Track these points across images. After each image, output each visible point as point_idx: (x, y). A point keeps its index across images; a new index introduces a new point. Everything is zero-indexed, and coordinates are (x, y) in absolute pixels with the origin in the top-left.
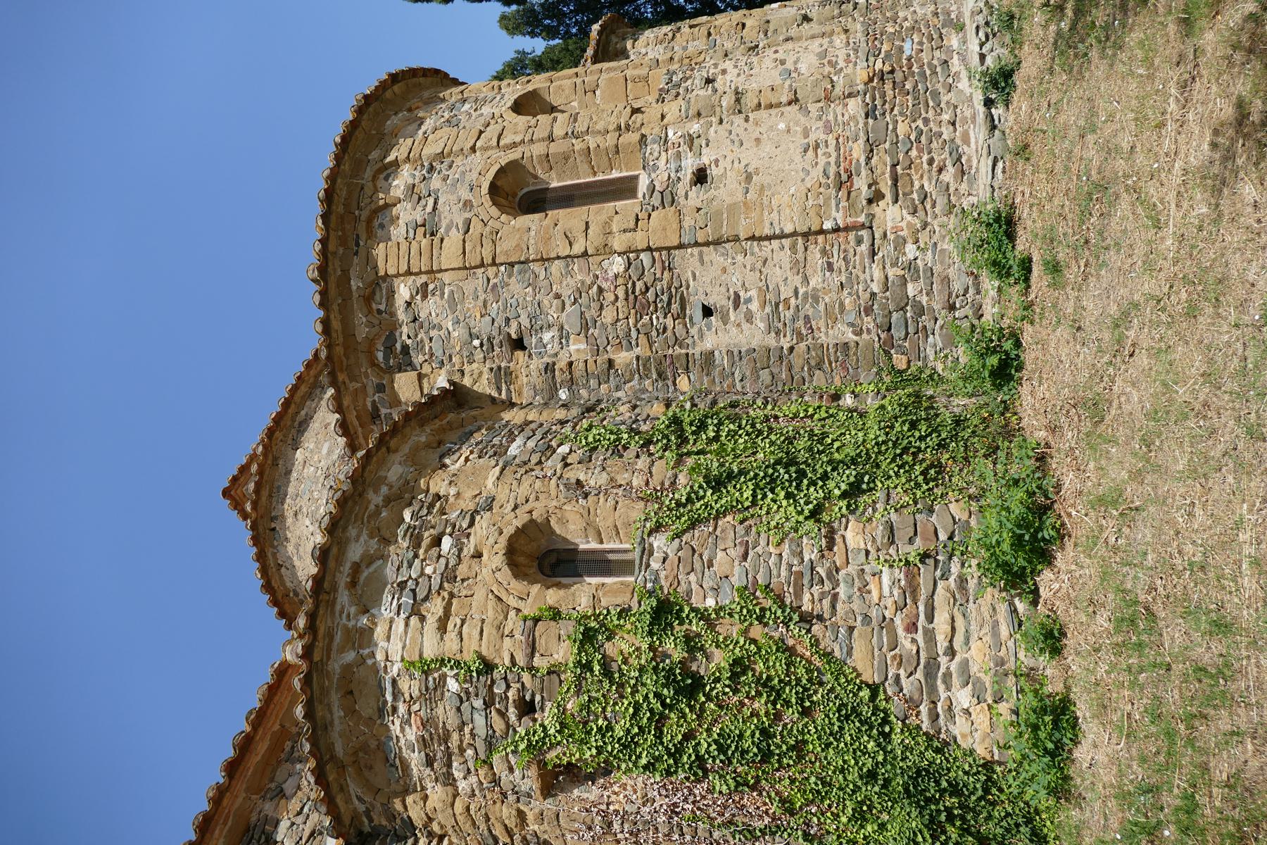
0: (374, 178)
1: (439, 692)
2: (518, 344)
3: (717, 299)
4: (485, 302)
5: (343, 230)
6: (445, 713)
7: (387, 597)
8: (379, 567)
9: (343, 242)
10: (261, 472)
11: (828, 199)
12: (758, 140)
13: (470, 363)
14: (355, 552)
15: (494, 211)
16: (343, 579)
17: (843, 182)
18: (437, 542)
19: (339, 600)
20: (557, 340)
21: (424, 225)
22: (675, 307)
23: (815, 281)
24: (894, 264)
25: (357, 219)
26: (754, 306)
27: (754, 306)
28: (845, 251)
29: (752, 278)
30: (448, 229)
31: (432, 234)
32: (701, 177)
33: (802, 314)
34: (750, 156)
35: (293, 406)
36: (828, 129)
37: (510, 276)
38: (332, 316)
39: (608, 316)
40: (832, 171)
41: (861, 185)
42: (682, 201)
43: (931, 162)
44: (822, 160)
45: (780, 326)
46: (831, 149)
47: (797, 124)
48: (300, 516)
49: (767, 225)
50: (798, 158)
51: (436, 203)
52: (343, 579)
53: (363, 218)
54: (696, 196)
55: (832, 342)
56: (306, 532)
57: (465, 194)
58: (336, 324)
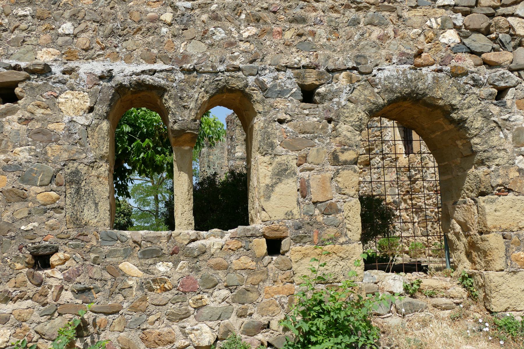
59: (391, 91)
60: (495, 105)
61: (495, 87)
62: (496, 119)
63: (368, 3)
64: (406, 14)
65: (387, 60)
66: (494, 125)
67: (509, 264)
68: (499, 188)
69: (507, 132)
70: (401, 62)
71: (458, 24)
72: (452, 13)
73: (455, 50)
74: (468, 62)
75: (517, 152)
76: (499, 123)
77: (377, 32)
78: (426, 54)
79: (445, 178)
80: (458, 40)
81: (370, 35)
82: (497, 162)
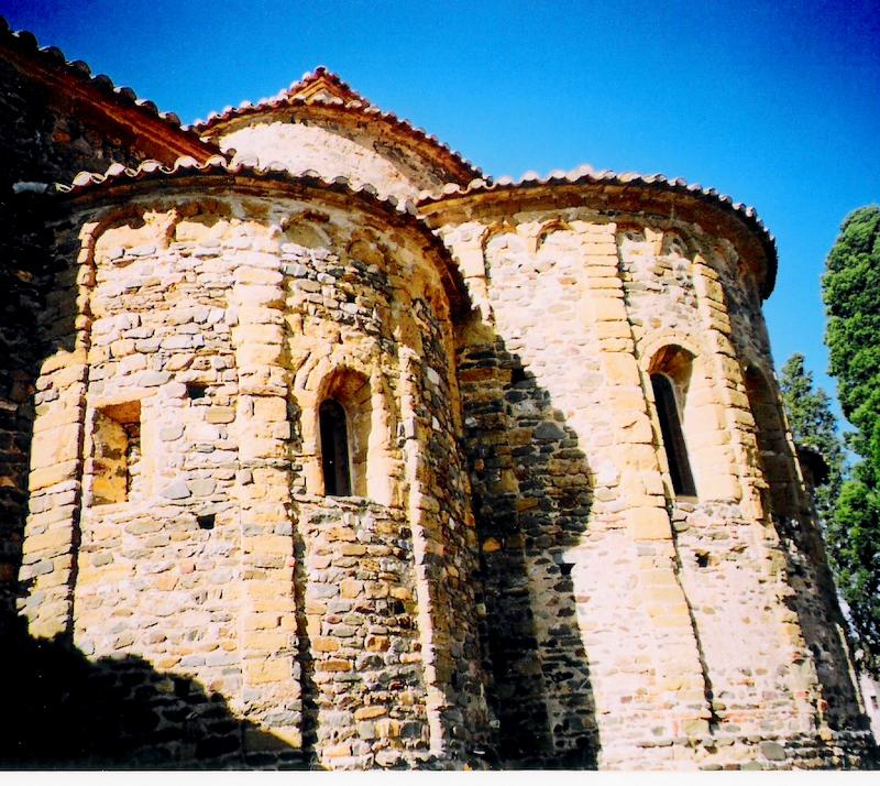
0: (676, 230)
1: (207, 300)
5: (624, 200)
6: (184, 306)
7: (298, 249)
8: (323, 242)
9: (613, 199)
10: (352, 110)
14: (338, 217)
16: (314, 206)
19: (292, 202)
25: (635, 211)
28: (644, 716)
35: (416, 142)
38: (540, 189)
45: (559, 646)
52: (314, 206)
53: (637, 219)
55: (546, 701)
58: (531, 192)
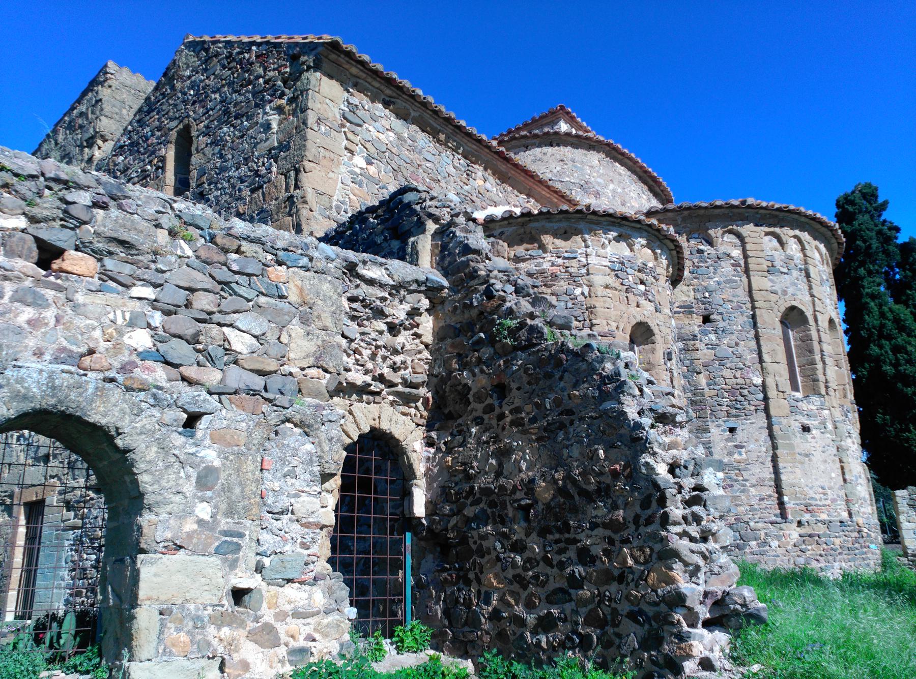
2: (706, 319)
3: (740, 435)
4: (731, 301)
11: (799, 499)
12: (826, 461)
13: (694, 290)
15: (783, 309)
17: (808, 509)
18: (642, 282)
20: (710, 342)
21: (773, 266)
22: (734, 411)
23: (753, 491)
24: (766, 534)
26: (736, 457)
27: (736, 457)
29: (753, 456)
30: (772, 281)
31: (768, 271)
32: (806, 429)
33: (733, 483)
34: (817, 457)
36: (833, 501)
37: (747, 317)
39: (727, 373)
40: (813, 502)
41: (806, 517)
42: (793, 418)
43: (821, 555)
44: (818, 496)
46: (824, 502)
47: (835, 484)
48: (561, 163)
49: (785, 465)
50: (818, 483)
51: (785, 273)
54: (796, 426)
56: (552, 166)
57: (790, 290)
59: (25, 398)
60: (180, 433)
61: (185, 411)
62: (176, 452)
63: (23, 273)
64: (80, 298)
65: (35, 354)
66: (173, 459)
67: (161, 651)
68: (166, 544)
69: (191, 470)
70: (56, 360)
71: (153, 324)
72: (150, 309)
73: (144, 356)
74: (159, 374)
75: (199, 498)
76: (182, 458)
77: (27, 313)
78: (99, 355)
79: (115, 524)
80: (151, 345)
81: (16, 316)
82: (169, 508)
